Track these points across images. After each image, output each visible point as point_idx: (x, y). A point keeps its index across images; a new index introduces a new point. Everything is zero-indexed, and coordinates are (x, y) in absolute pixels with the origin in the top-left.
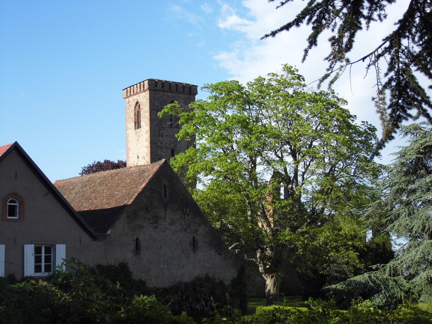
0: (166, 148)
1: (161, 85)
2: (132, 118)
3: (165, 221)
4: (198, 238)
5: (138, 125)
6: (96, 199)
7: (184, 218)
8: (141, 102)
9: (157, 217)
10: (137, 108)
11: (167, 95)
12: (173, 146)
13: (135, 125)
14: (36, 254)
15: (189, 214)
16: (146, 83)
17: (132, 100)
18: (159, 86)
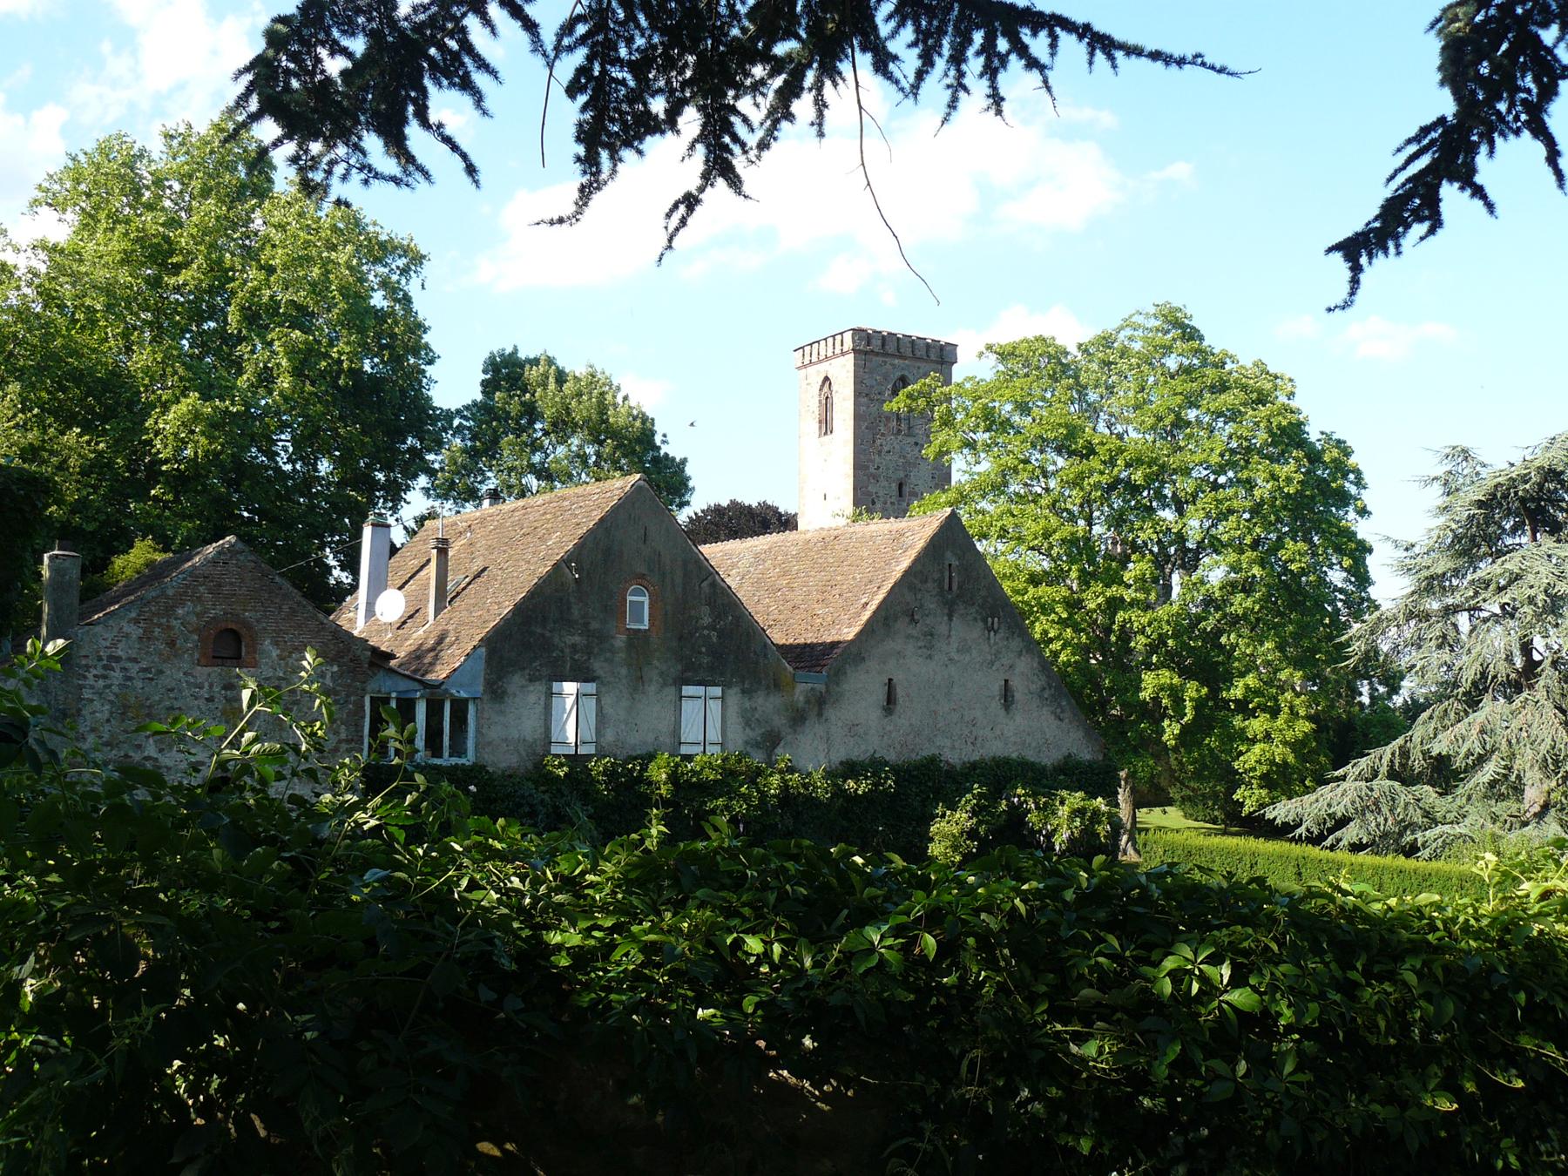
0: (887, 478)
1: (879, 342)
3: (949, 644)
4: (1016, 683)
5: (826, 425)
6: (792, 589)
9: (932, 635)
10: (826, 389)
11: (891, 364)
12: (902, 474)
13: (820, 428)
16: (848, 337)
17: (816, 374)
18: (876, 343)
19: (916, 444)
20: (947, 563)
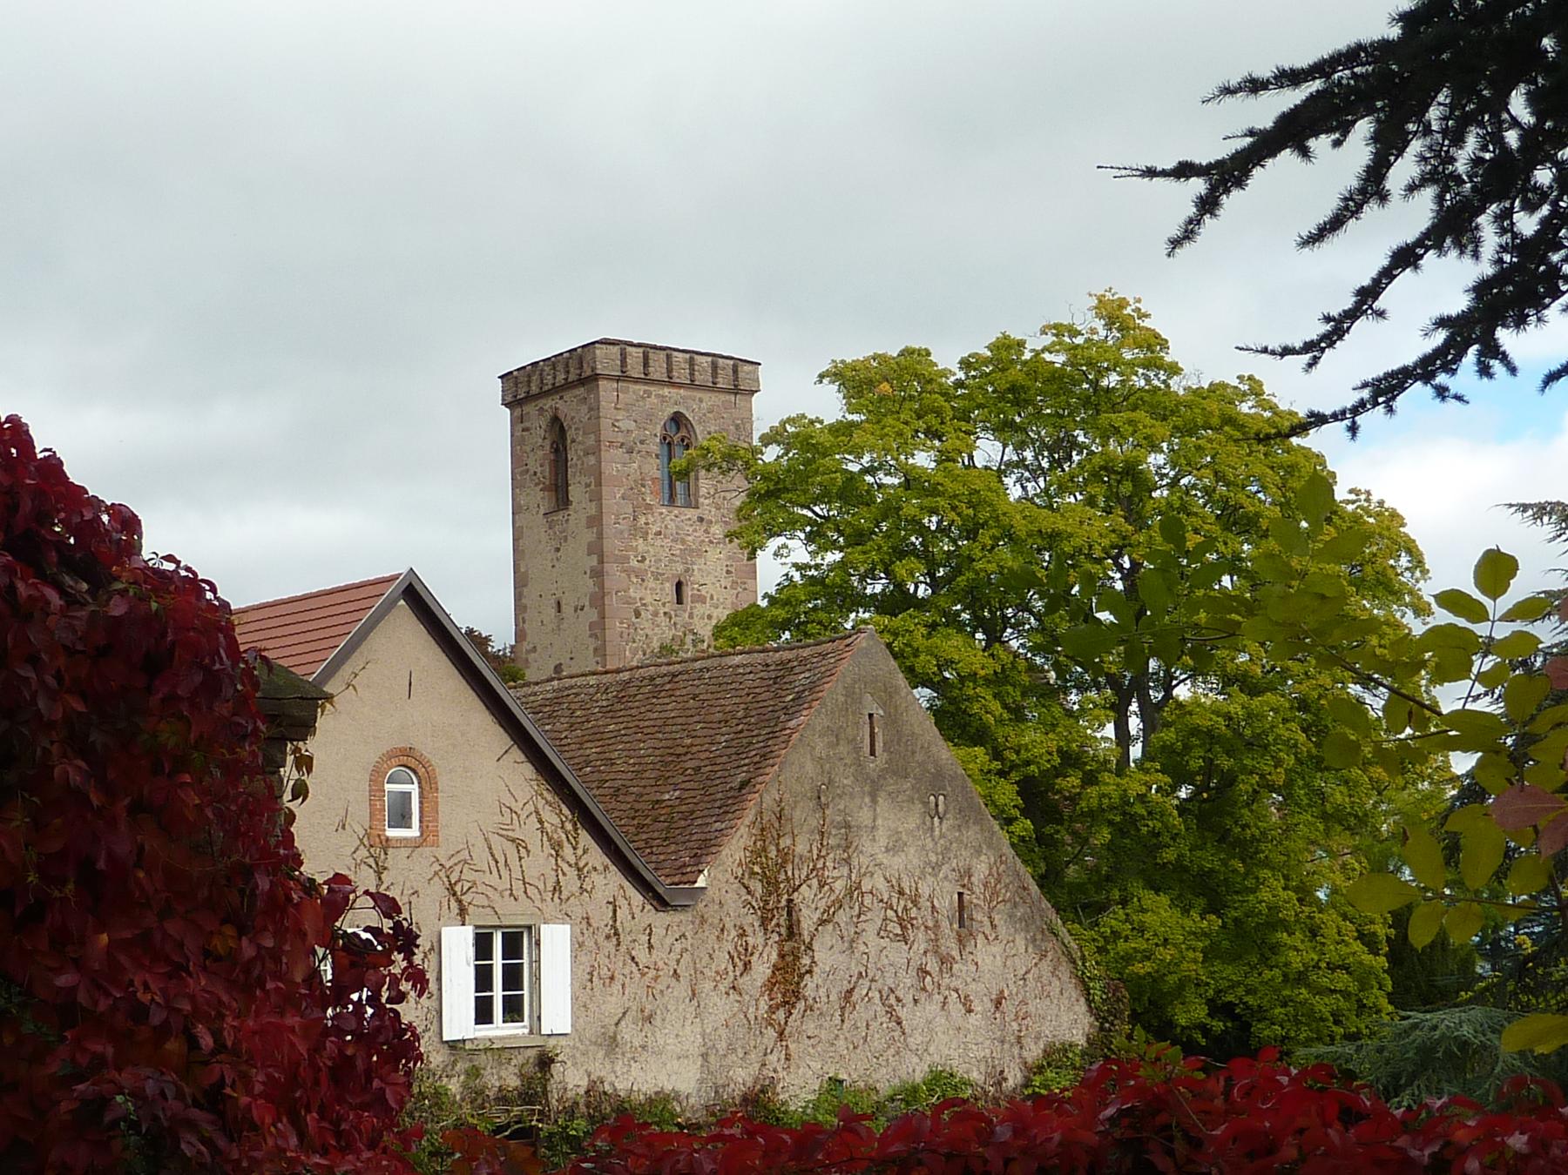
2: (535, 473)
7: (932, 829)
8: (569, 418)
9: (848, 826)
12: (680, 568)
14: (476, 960)
15: (945, 815)
19: (701, 520)
20: (866, 713)
